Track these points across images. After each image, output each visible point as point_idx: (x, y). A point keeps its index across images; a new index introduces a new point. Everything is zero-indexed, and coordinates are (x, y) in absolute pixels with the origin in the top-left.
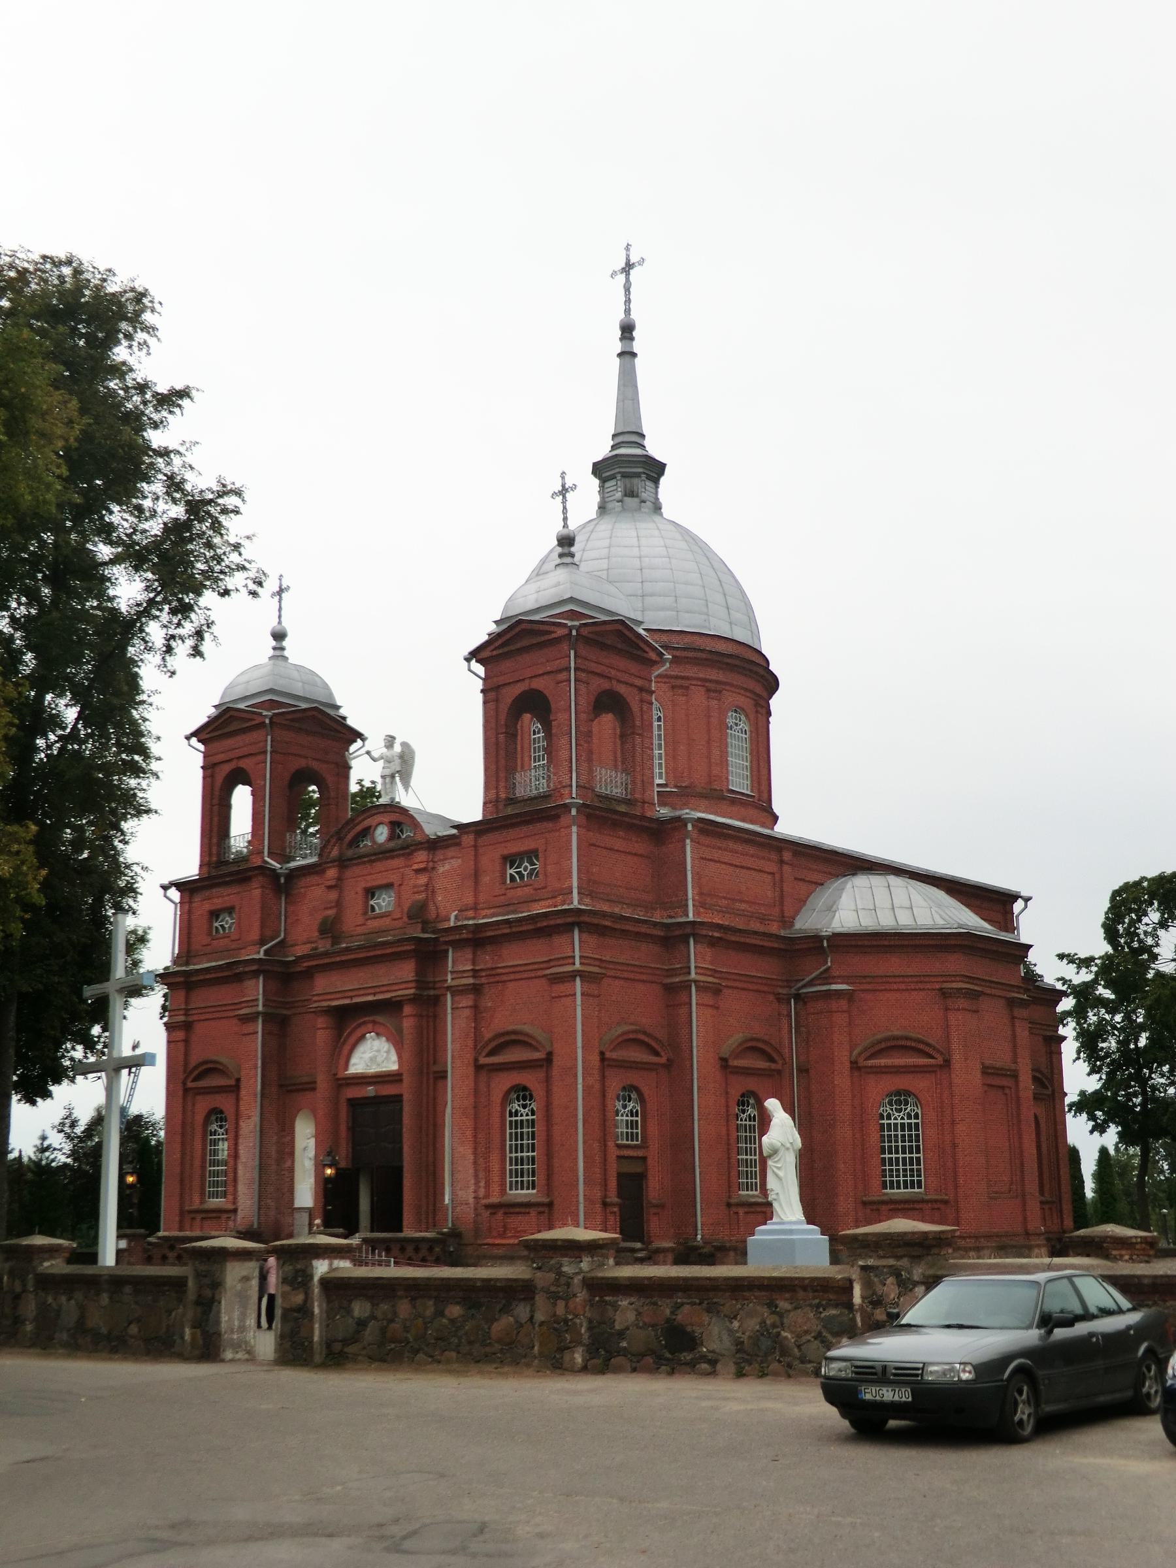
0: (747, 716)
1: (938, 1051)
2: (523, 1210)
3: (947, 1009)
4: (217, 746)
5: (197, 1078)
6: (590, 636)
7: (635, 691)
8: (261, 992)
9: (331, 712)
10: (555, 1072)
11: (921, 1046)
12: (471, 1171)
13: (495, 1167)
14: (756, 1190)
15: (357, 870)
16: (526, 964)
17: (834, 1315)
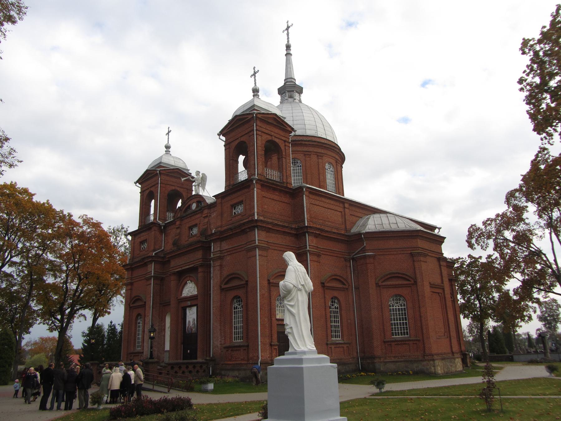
0: (333, 166)
1: (412, 278)
3: (414, 261)
6: (262, 118)
7: (283, 142)
8: (153, 268)
11: (404, 276)
14: (340, 338)
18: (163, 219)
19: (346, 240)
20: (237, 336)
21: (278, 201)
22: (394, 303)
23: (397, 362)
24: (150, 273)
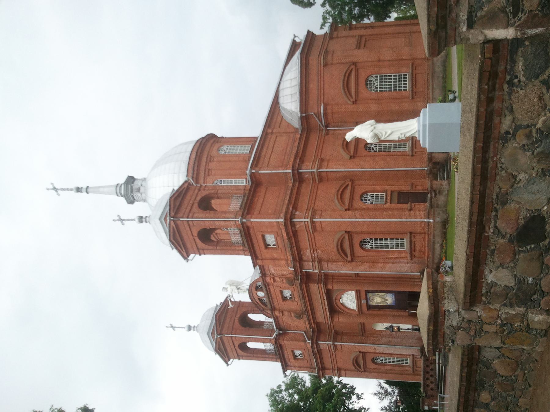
0: (221, 146)
2: (413, 244)
3: (332, 64)
4: (230, 354)
5: (360, 367)
7: (200, 192)
9: (219, 308)
10: (354, 230)
11: (347, 75)
12: (396, 264)
13: (394, 255)
14: (406, 144)
15: (276, 304)
16: (309, 241)
17: (523, 65)
18: (270, 332)
19: (307, 134)
20: (400, 245)
21: (264, 199)
22: (373, 87)
23: (433, 87)
24: (329, 346)
